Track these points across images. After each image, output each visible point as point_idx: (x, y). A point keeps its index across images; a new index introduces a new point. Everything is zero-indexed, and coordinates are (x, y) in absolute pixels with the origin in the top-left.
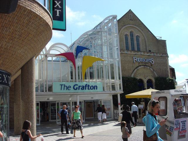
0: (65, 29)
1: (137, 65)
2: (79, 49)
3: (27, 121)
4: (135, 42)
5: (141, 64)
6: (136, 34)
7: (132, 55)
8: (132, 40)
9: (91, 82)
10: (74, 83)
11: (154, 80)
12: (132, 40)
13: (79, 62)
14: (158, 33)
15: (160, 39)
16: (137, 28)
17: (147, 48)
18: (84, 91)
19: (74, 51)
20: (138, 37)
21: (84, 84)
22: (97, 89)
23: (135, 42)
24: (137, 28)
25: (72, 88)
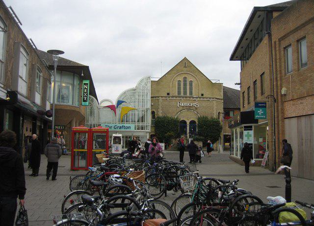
0: (289, 162)
1: (181, 108)
2: (120, 103)
3: (22, 169)
4: (188, 87)
5: (184, 108)
6: (189, 79)
7: (177, 101)
8: (185, 85)
9: (126, 125)
10: (115, 125)
11: (196, 121)
12: (185, 85)
13: (118, 111)
14: (26, 187)
15: (218, 82)
16: (191, 73)
17: (200, 92)
18: (121, 129)
19: (115, 103)
20: (191, 82)
21: (121, 125)
22: (54, 179)
23: (188, 87)
24: (191, 73)
25: (113, 127)
